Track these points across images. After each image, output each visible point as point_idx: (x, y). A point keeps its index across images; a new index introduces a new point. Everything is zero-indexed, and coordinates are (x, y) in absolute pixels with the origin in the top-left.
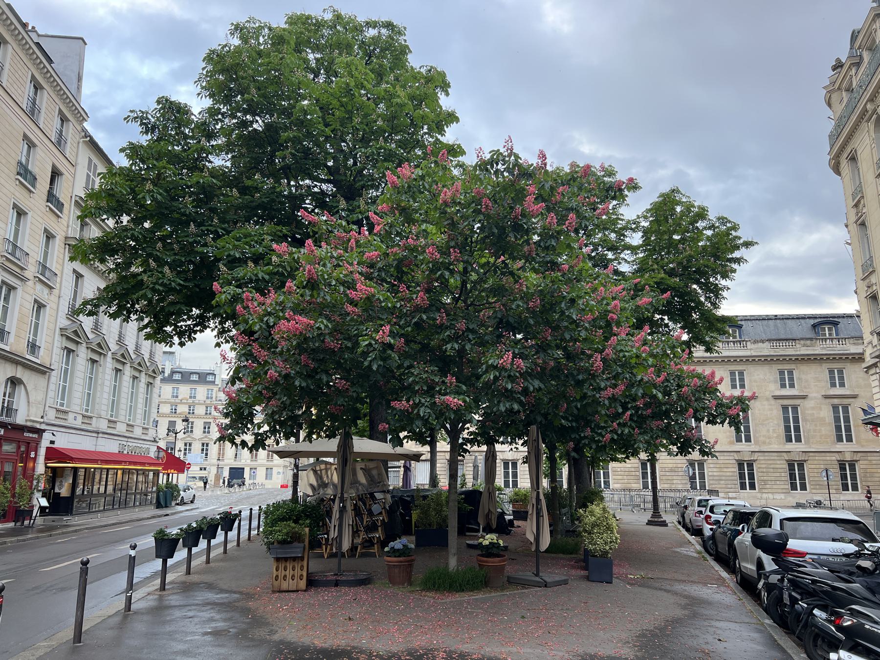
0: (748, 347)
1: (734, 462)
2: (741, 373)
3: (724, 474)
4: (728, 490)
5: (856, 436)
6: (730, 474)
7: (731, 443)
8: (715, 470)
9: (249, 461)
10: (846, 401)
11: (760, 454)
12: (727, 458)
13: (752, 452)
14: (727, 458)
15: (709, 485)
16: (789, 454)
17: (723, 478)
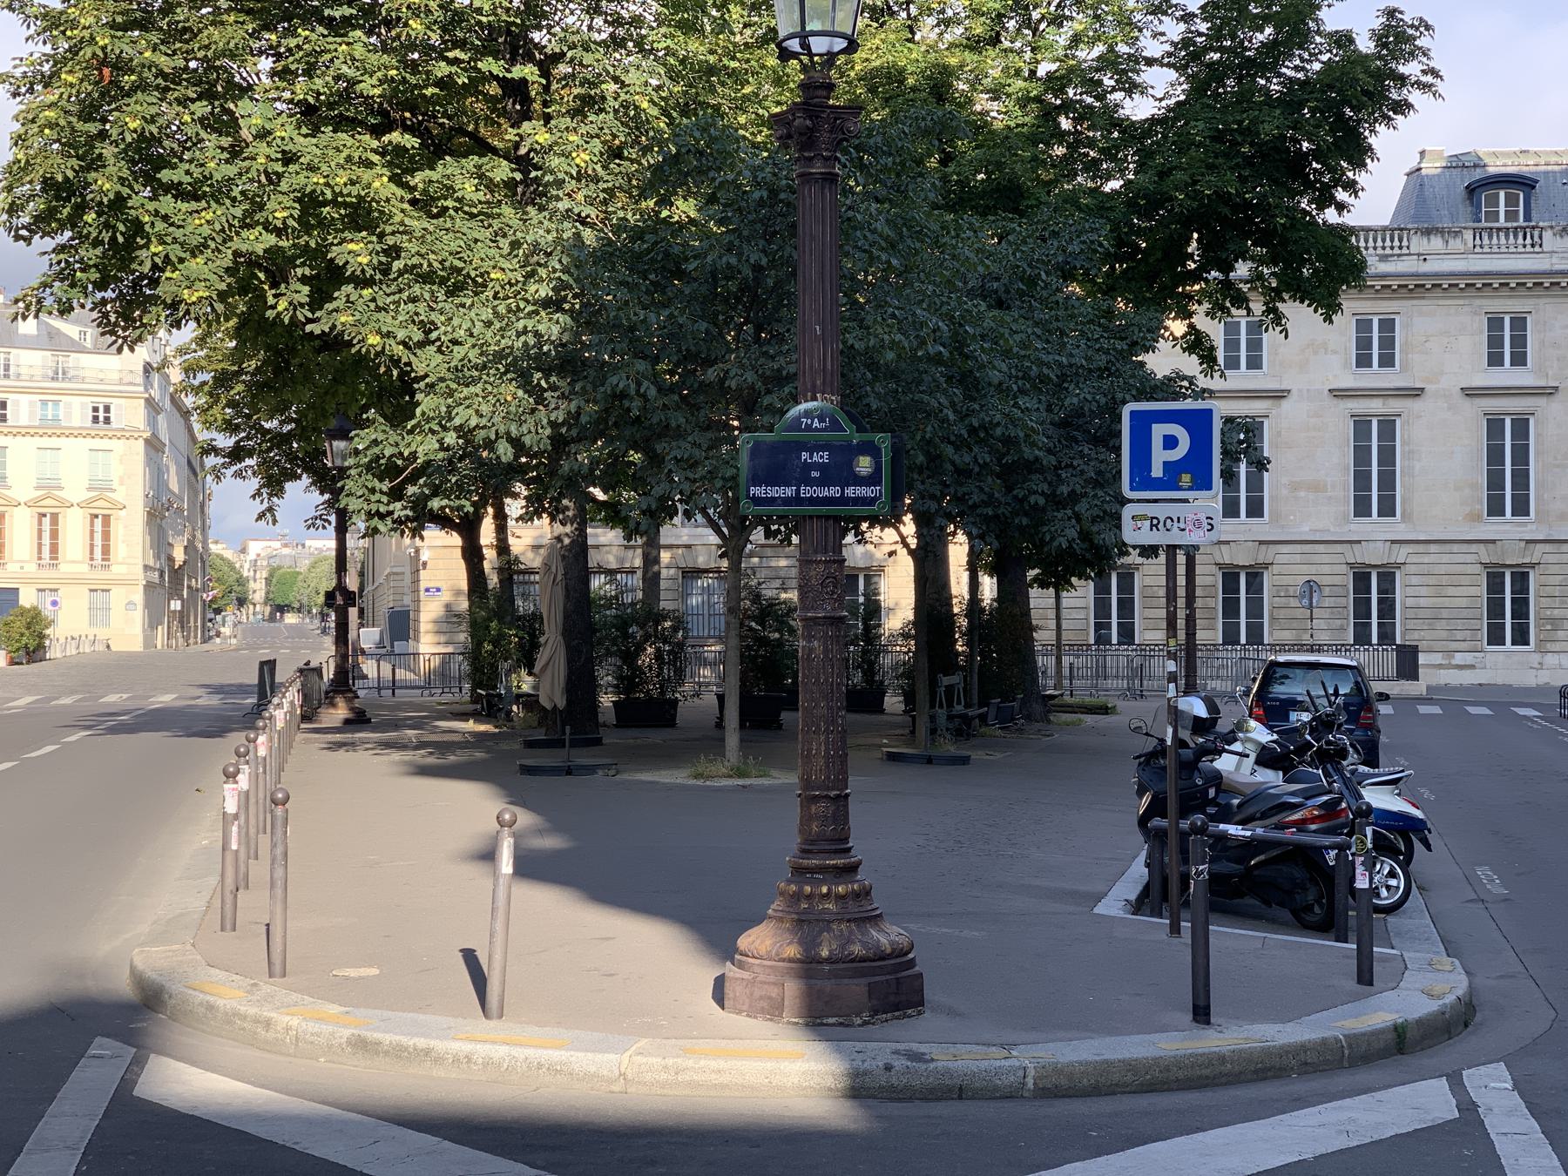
0: (1545, 248)
1: (1478, 569)
2: (1519, 323)
3: (1446, 602)
4: (1454, 646)
5: (1537, 498)
6: (1464, 602)
7: (1474, 518)
8: (1424, 591)
9: (31, 568)
10: (1394, 406)
11: (1548, 548)
12: (1460, 558)
13: (1528, 542)
14: (1460, 558)
15: (1405, 631)
16: (1491, 546)
17: (1445, 614)
